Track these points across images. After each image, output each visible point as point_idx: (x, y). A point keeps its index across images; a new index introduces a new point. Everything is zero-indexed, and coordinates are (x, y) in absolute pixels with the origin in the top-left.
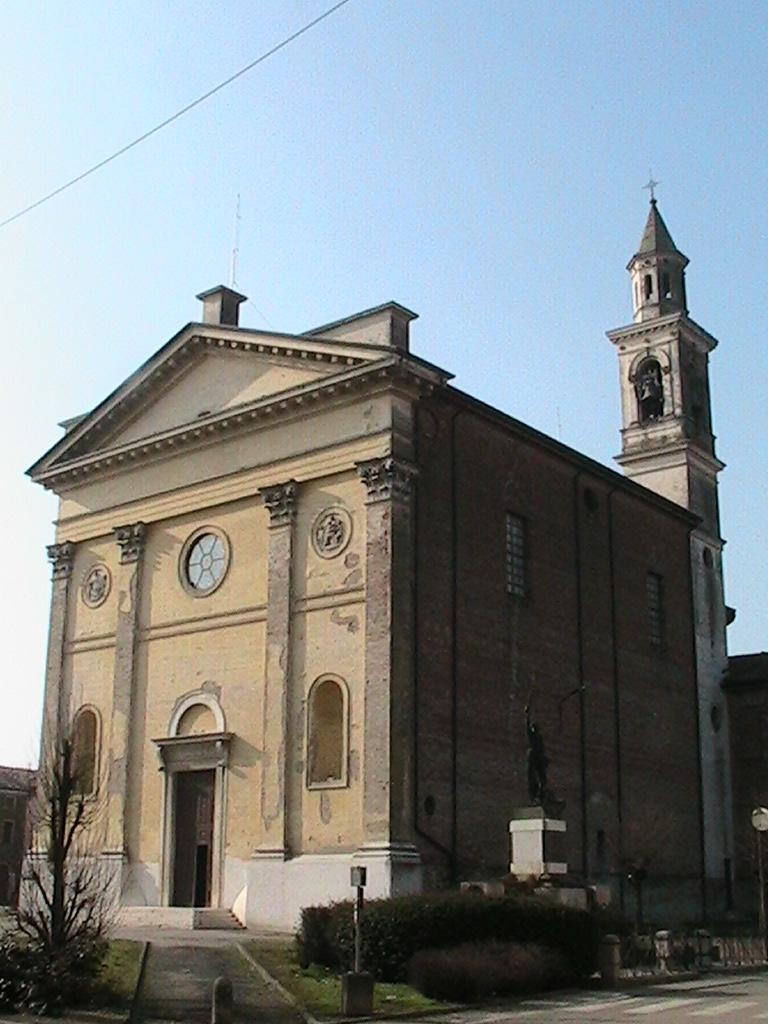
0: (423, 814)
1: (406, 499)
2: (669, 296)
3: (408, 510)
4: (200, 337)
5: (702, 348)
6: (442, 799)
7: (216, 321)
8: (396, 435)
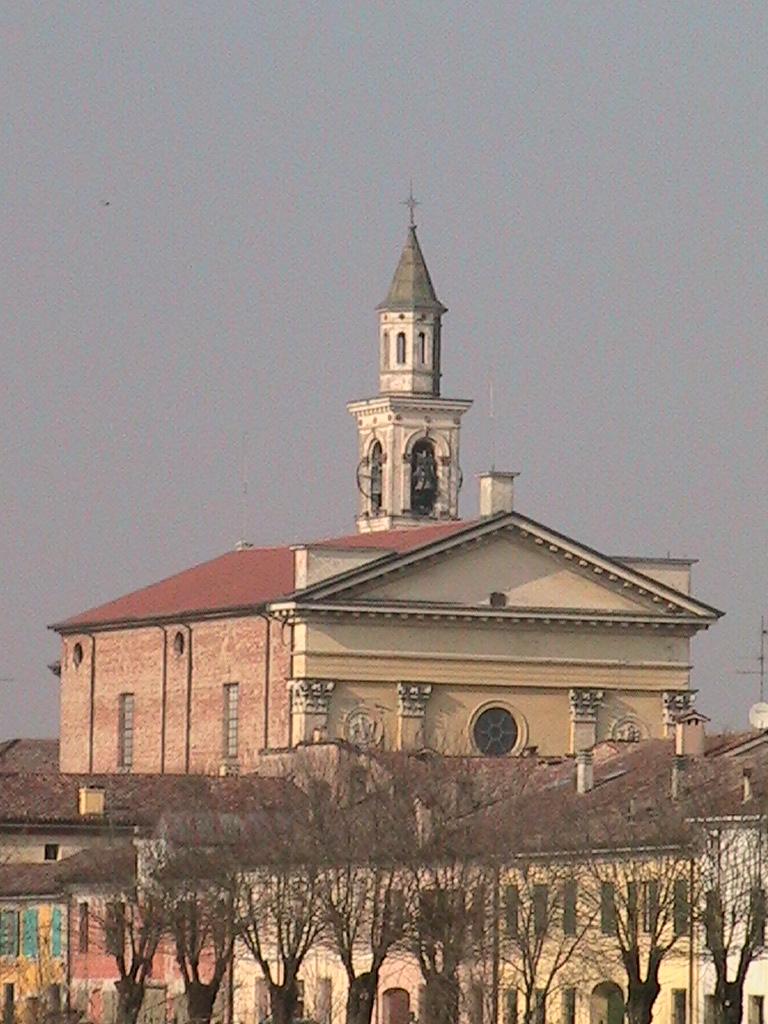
4: (515, 526)
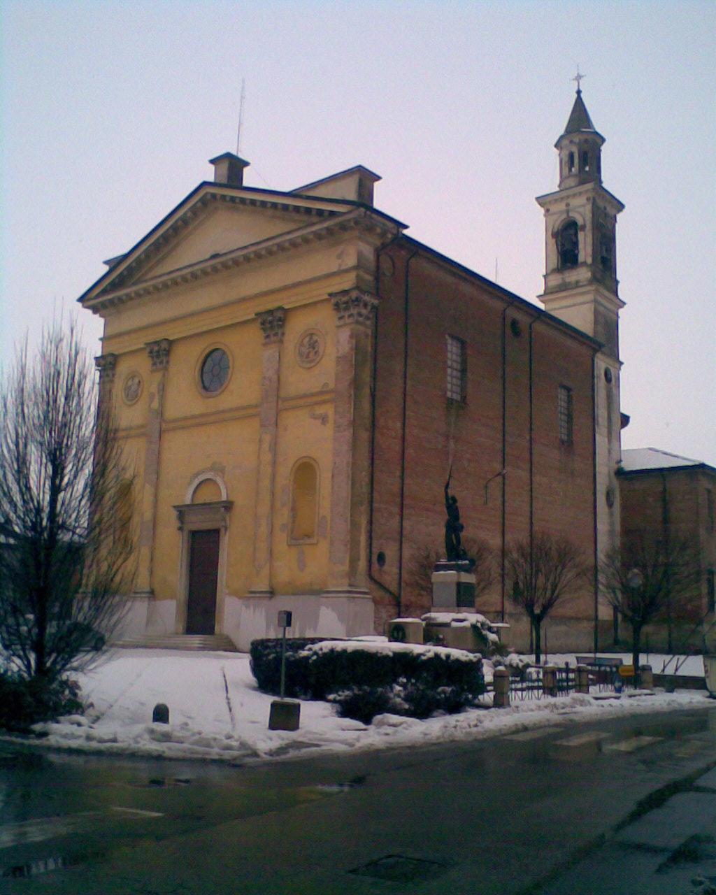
0: (376, 566)
1: (368, 323)
2: (587, 169)
3: (369, 332)
5: (610, 211)
6: (391, 553)
7: (224, 181)
8: (361, 273)
